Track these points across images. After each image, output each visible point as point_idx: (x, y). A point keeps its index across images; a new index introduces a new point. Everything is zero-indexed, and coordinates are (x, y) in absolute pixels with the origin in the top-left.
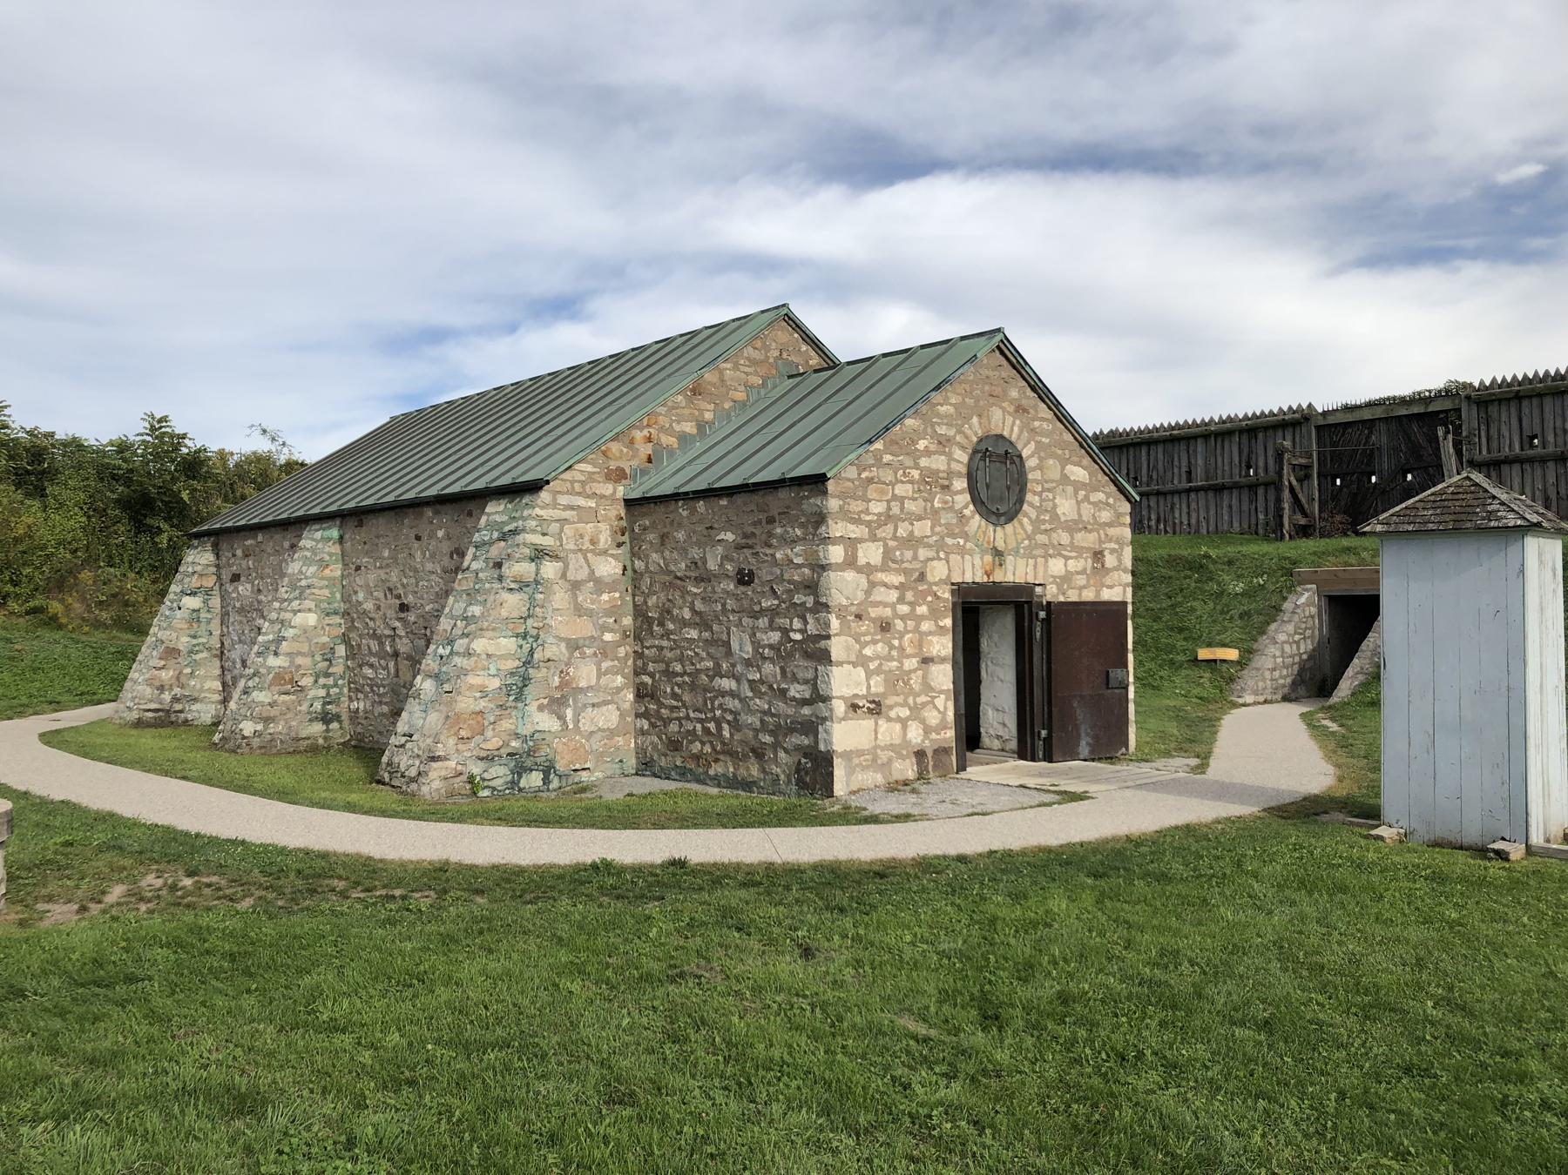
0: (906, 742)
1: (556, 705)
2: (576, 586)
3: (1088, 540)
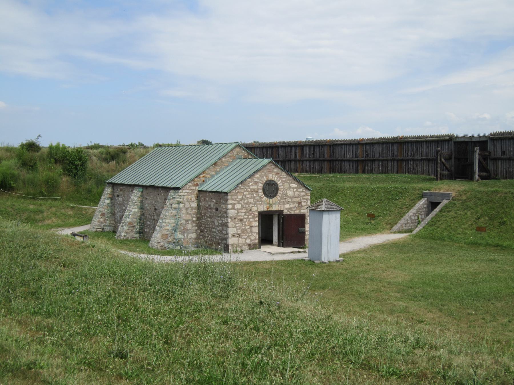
1: (183, 233)
2: (187, 209)
3: (298, 200)
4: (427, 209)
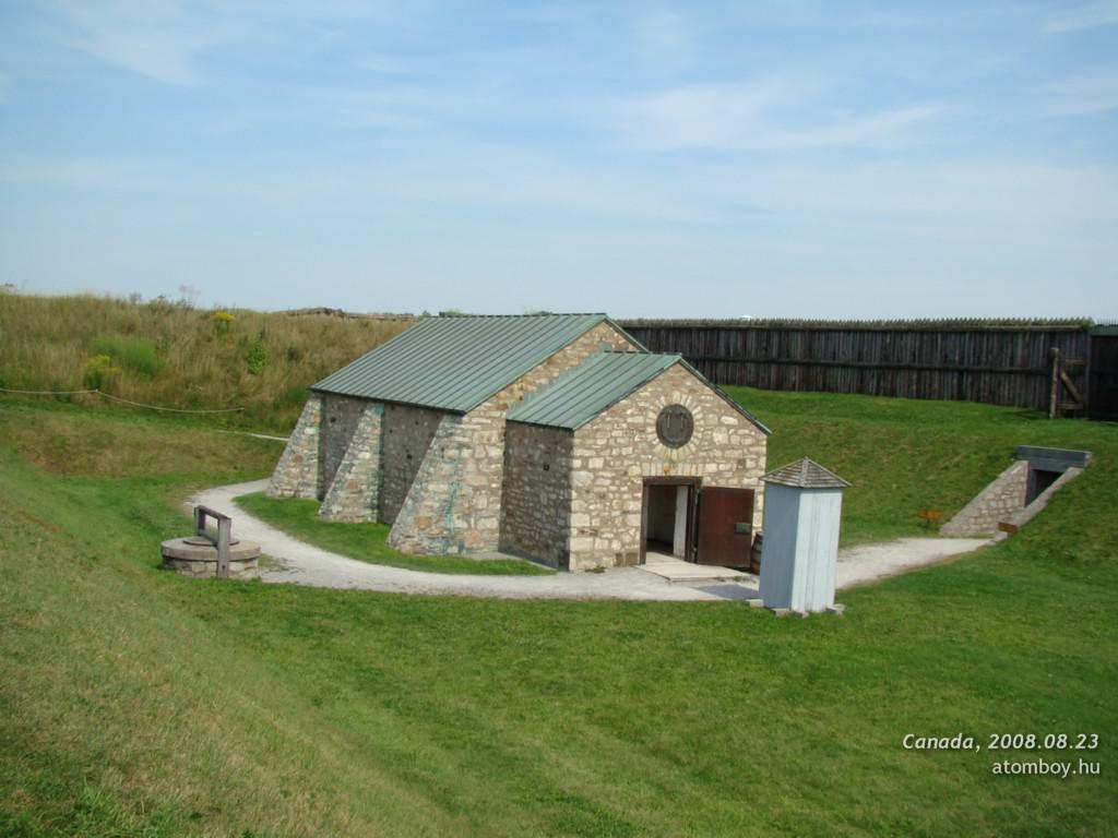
0: (610, 549)
1: (466, 516)
2: (478, 461)
3: (737, 454)
4: (1025, 487)
